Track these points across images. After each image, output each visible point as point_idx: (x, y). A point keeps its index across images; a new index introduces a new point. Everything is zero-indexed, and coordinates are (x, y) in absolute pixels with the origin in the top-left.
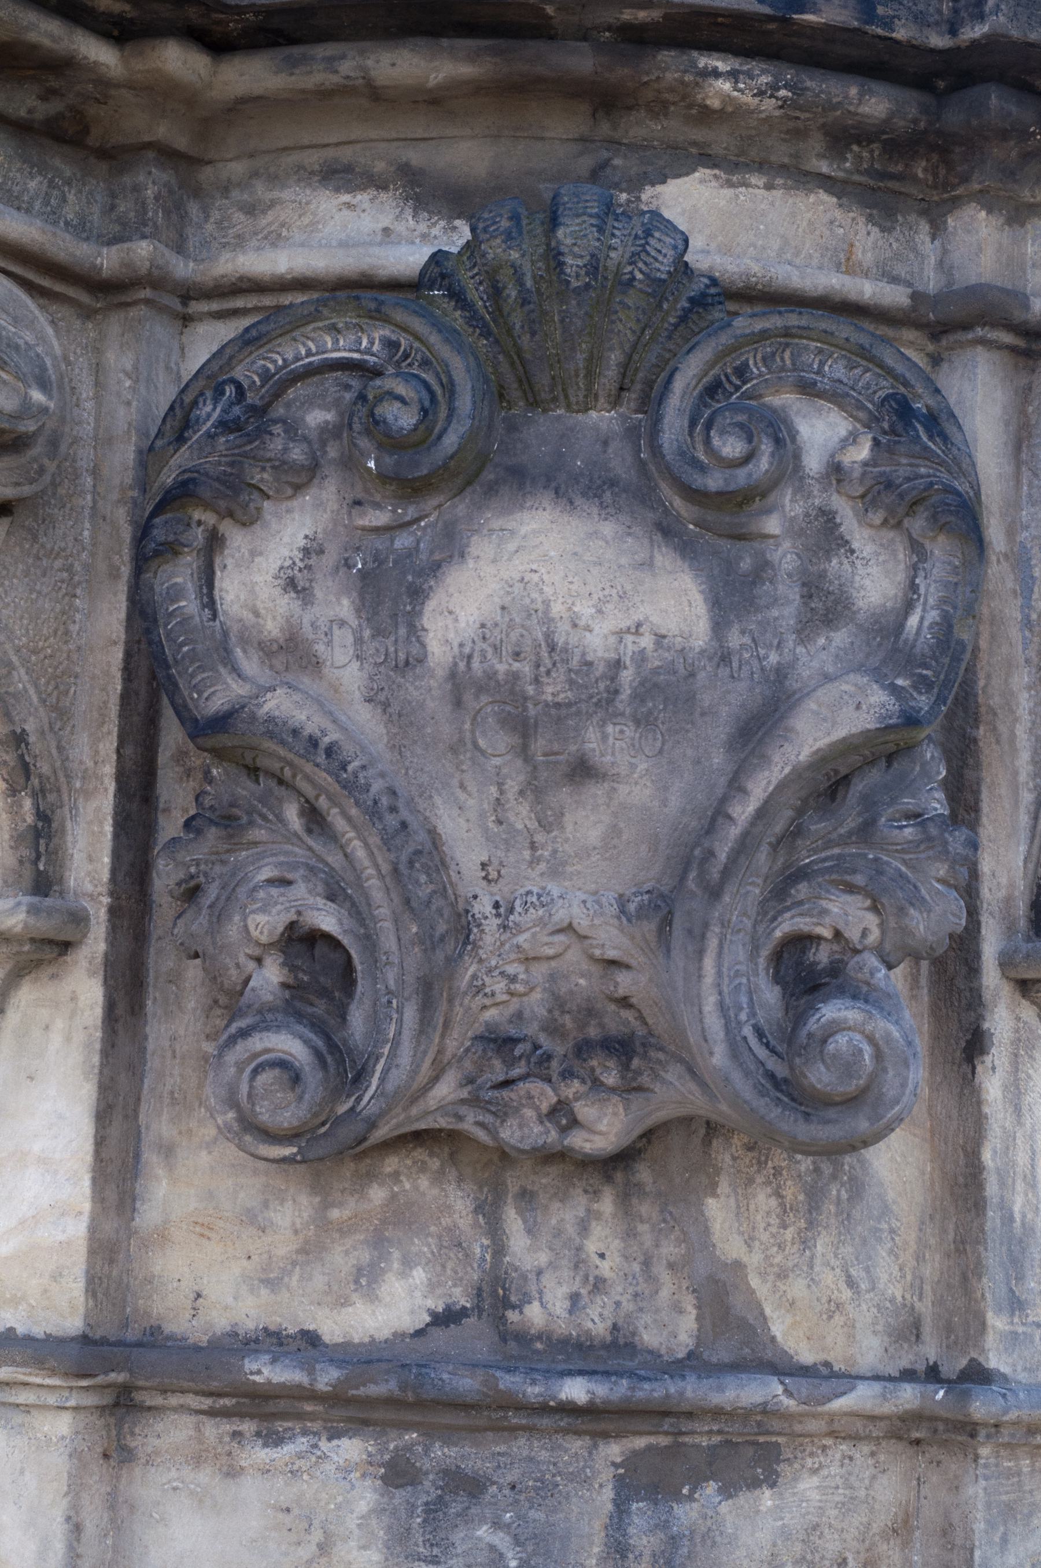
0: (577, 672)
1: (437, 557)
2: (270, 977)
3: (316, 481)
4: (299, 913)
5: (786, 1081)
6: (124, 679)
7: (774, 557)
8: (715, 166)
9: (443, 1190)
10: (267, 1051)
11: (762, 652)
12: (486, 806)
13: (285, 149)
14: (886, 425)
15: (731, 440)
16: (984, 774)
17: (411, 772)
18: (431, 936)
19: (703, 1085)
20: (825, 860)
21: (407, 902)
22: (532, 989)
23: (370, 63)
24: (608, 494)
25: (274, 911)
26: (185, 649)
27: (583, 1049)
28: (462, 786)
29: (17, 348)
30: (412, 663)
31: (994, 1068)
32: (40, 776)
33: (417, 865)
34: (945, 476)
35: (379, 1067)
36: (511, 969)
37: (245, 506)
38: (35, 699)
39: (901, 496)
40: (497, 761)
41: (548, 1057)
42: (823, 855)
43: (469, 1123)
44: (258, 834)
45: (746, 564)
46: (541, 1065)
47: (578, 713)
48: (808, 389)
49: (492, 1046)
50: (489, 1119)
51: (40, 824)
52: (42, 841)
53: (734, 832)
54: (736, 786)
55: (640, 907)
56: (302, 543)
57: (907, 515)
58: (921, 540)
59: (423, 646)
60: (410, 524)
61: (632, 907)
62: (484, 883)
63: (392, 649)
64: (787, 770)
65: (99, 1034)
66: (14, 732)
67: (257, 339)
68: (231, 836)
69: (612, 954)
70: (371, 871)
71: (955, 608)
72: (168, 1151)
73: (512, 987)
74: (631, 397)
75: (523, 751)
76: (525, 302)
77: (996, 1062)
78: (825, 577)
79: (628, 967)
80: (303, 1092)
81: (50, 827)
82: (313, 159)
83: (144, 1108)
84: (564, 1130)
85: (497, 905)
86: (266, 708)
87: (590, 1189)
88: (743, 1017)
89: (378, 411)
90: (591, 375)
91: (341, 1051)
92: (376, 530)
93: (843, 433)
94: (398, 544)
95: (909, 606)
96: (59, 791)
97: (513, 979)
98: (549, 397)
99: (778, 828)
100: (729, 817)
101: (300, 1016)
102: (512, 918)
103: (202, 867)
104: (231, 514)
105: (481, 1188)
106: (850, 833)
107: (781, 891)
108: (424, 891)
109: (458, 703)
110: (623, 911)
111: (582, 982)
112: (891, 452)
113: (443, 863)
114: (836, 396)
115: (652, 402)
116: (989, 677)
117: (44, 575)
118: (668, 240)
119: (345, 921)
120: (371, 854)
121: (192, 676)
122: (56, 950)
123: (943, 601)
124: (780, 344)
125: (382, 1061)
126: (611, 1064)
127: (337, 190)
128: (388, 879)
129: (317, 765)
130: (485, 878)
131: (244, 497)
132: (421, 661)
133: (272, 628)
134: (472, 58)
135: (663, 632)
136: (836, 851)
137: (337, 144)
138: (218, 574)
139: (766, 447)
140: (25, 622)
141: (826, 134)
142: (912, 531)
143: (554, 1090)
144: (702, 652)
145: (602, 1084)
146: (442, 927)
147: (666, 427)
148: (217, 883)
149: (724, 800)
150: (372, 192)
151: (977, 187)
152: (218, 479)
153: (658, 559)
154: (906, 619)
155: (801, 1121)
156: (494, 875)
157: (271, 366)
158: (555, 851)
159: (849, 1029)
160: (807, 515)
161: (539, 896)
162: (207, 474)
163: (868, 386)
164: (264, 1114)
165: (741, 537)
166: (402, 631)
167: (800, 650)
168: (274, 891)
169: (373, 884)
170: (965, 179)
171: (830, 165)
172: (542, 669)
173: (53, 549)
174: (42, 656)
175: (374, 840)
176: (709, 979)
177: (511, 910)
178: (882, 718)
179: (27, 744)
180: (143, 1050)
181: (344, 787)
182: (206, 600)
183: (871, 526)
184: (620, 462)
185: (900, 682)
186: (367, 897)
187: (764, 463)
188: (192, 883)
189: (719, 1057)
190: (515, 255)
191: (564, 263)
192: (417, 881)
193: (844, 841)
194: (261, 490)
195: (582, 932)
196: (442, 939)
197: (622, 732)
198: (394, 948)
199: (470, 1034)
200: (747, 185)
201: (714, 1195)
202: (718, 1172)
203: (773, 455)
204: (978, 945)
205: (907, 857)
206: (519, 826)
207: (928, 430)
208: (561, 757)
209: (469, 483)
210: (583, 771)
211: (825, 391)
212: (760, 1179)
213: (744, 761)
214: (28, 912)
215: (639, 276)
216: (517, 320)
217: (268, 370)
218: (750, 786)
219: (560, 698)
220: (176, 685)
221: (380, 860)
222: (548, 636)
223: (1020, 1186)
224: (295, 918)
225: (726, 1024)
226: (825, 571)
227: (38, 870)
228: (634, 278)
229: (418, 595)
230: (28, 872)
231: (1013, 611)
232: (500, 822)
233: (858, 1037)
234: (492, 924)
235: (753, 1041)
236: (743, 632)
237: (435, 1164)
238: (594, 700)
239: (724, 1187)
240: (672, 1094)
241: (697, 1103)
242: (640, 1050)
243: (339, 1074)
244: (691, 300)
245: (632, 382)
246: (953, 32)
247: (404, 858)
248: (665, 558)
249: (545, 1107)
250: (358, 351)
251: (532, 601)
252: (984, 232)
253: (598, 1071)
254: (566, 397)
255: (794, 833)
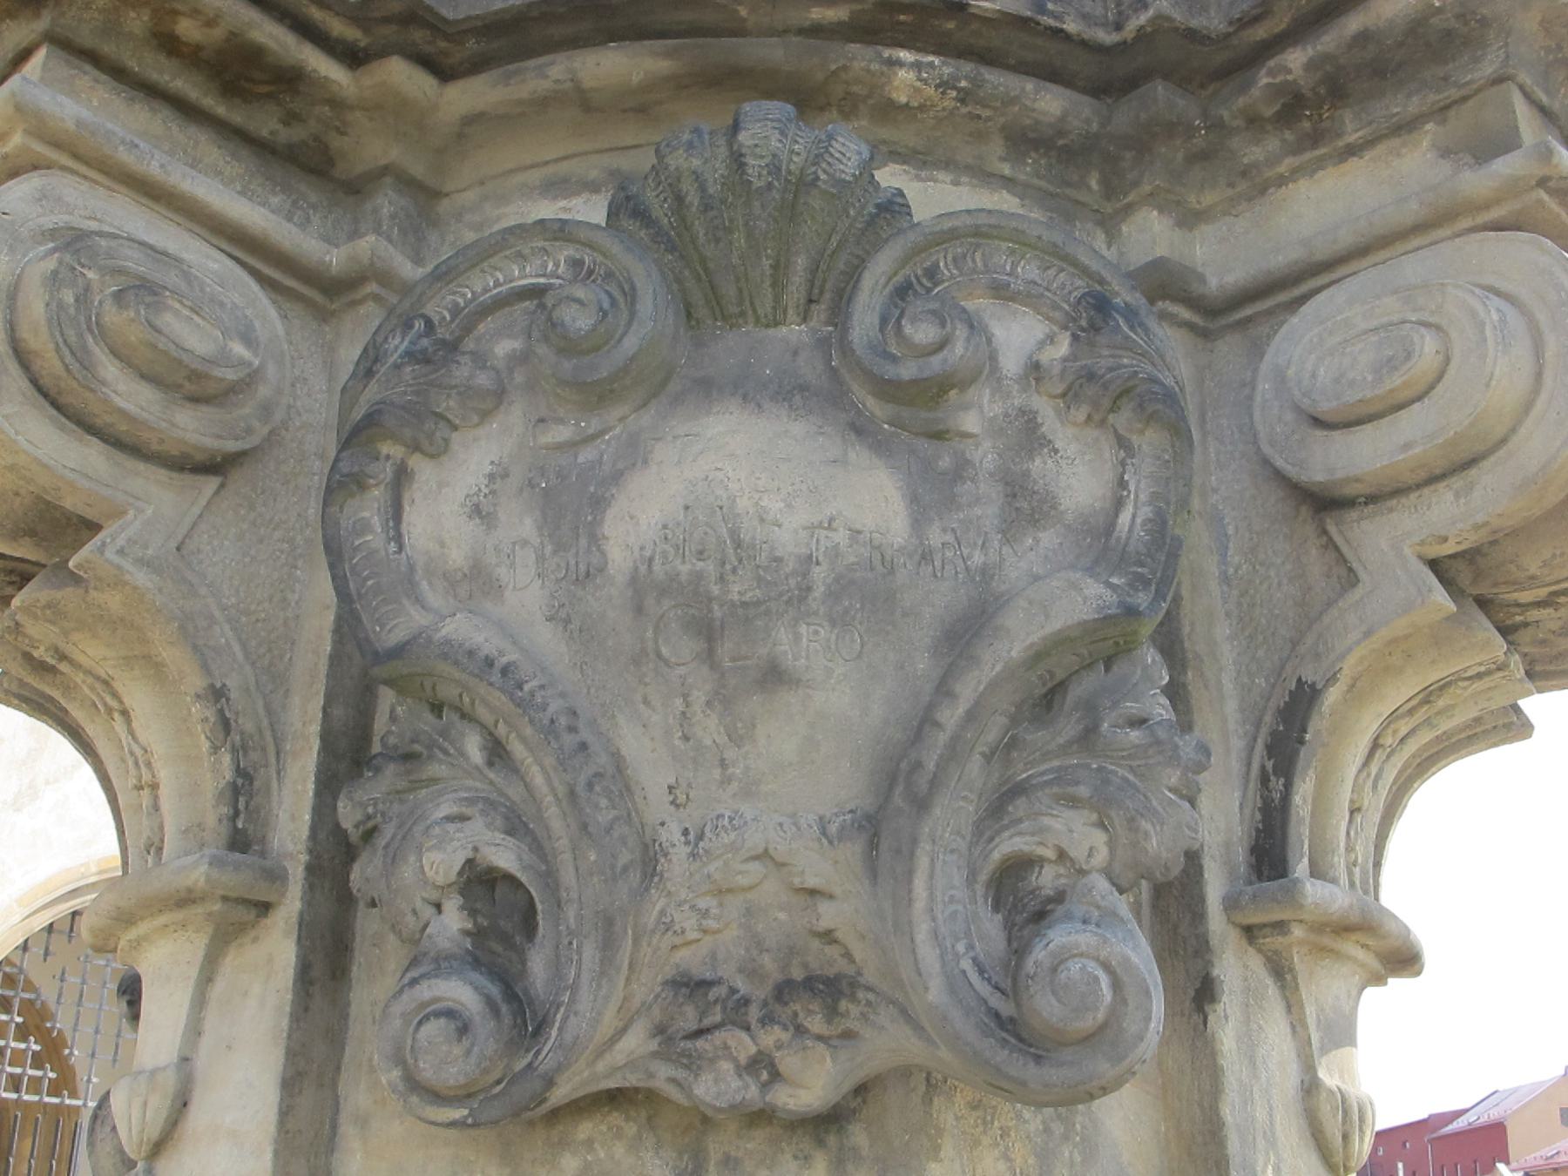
0: (766, 569)
1: (620, 466)
2: (452, 923)
3: (502, 408)
4: (476, 849)
5: (1012, 1020)
6: (334, 642)
7: (975, 456)
8: (904, 163)
9: (640, 1158)
10: (436, 1000)
11: (966, 552)
12: (671, 721)
13: (511, 171)
14: (1084, 323)
15: (924, 326)
16: (1195, 716)
17: (593, 690)
18: (613, 867)
19: (918, 1028)
20: (1043, 774)
21: (584, 827)
22: (727, 925)
23: (577, 65)
24: (798, 397)
25: (449, 849)
26: (370, 583)
27: (784, 991)
28: (646, 701)
29: (222, 305)
30: (589, 576)
31: (1226, 1017)
32: (242, 733)
33: (597, 788)
34: (1149, 368)
35: (559, 1016)
36: (702, 904)
37: (430, 436)
38: (240, 656)
39: (1105, 386)
40: (681, 670)
41: (746, 1002)
42: (1043, 768)
43: (662, 1075)
44: (436, 769)
45: (945, 463)
46: (737, 1012)
47: (768, 612)
48: (1001, 292)
49: (684, 990)
50: (680, 1074)
51: (240, 781)
52: (242, 800)
53: (943, 738)
54: (944, 690)
55: (842, 828)
56: (488, 469)
57: (1112, 410)
58: (1127, 435)
59: (603, 554)
60: (594, 437)
61: (833, 829)
62: (672, 808)
63: (573, 562)
64: (998, 668)
65: (290, 996)
66: (212, 686)
67: (446, 273)
68: (409, 772)
69: (811, 882)
70: (550, 798)
71: (1168, 504)
72: (363, 1121)
73: (704, 922)
74: (820, 312)
75: (709, 656)
76: (706, 208)
77: (1229, 1011)
78: (1029, 476)
79: (831, 897)
80: (473, 1045)
81: (251, 783)
82: (535, 176)
83: (344, 1075)
84: (765, 1086)
85: (686, 832)
86: (444, 632)
87: (800, 1155)
88: (961, 948)
89: (556, 314)
90: (778, 285)
91: (520, 1001)
92: (559, 447)
93: (1041, 336)
94: (581, 459)
95: (1119, 504)
96: (264, 749)
97: (705, 914)
98: (736, 310)
99: (992, 735)
100: (937, 724)
101: (476, 963)
102: (701, 844)
103: (380, 806)
104: (416, 448)
105: (680, 1154)
106: (1070, 743)
107: (999, 807)
108: (604, 817)
109: (639, 610)
110: (824, 833)
111: (782, 916)
112: (1092, 344)
113: (628, 789)
114: (1029, 297)
115: (840, 313)
116: (1192, 624)
117: (261, 541)
118: (852, 146)
119: (525, 857)
120: (548, 780)
121: (376, 609)
122: (253, 912)
123: (1155, 496)
124: (971, 244)
125: (562, 1010)
126: (815, 1007)
127: (555, 198)
128: (564, 803)
129: (491, 684)
130: (672, 803)
131: (429, 425)
132: (601, 570)
133: (457, 557)
134: (668, 54)
135: (858, 527)
136: (1056, 763)
137: (557, 160)
138: (407, 508)
139: (961, 332)
140: (236, 583)
141: (1007, 138)
142: (1117, 426)
143: (753, 1038)
144: (901, 549)
145: (807, 1031)
146: (624, 858)
147: (855, 323)
148: (394, 823)
149: (931, 707)
150: (585, 196)
151: (1147, 188)
152: (403, 408)
153: (852, 455)
154: (1117, 516)
155: (1032, 1064)
156: (682, 799)
157: (461, 301)
158: (747, 768)
159: (1081, 955)
160: (1007, 415)
161: (731, 819)
162: (392, 404)
163: (1063, 287)
164: (427, 1070)
165: (939, 436)
166: (583, 542)
167: (1005, 550)
168: (451, 827)
169: (552, 812)
170: (1136, 184)
171: (1013, 167)
172: (728, 567)
173: (271, 520)
174: (253, 618)
175: (549, 761)
176: (920, 904)
177: (701, 837)
178: (1100, 609)
179: (228, 700)
180: (345, 1017)
181: (519, 705)
182: (392, 533)
183: (1075, 424)
184: (810, 369)
185: (1114, 580)
186: (547, 828)
187: (959, 348)
188: (370, 824)
189: (936, 992)
190: (696, 162)
191: (745, 164)
192: (597, 806)
193: (1064, 750)
194: (449, 421)
195: (779, 859)
196: (625, 869)
197: (816, 632)
198: (574, 881)
199: (659, 978)
200: (936, 181)
201: (937, 1159)
202: (940, 1132)
203: (968, 340)
204: (1201, 889)
205: (1134, 763)
206: (708, 742)
207: (1127, 320)
208: (749, 662)
209: (655, 395)
210: (774, 676)
211: (1019, 293)
212: (986, 1141)
213: (952, 664)
214: (211, 864)
215: (823, 177)
216: (700, 230)
217: (456, 304)
218: (958, 688)
219: (747, 598)
220: (359, 619)
221: (556, 783)
222: (734, 533)
223: (1261, 1143)
224: (470, 855)
225: (942, 956)
226: (1028, 470)
227: (235, 827)
228: (818, 178)
229: (599, 504)
230: (224, 830)
231: (1212, 566)
232: (686, 738)
233: (1092, 966)
234: (680, 852)
235: (974, 977)
236: (944, 530)
237: (631, 1129)
238: (785, 598)
239: (948, 1149)
240: (885, 1043)
241: (912, 1048)
242: (847, 991)
243: (515, 1025)
244: (878, 206)
245: (821, 293)
246: (1118, 27)
247: (582, 779)
248: (859, 455)
249: (743, 1059)
250: (543, 275)
251: (717, 498)
252: (1157, 228)
253: (801, 1015)
254: (755, 311)
255: (1008, 747)
